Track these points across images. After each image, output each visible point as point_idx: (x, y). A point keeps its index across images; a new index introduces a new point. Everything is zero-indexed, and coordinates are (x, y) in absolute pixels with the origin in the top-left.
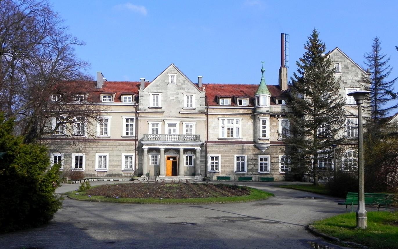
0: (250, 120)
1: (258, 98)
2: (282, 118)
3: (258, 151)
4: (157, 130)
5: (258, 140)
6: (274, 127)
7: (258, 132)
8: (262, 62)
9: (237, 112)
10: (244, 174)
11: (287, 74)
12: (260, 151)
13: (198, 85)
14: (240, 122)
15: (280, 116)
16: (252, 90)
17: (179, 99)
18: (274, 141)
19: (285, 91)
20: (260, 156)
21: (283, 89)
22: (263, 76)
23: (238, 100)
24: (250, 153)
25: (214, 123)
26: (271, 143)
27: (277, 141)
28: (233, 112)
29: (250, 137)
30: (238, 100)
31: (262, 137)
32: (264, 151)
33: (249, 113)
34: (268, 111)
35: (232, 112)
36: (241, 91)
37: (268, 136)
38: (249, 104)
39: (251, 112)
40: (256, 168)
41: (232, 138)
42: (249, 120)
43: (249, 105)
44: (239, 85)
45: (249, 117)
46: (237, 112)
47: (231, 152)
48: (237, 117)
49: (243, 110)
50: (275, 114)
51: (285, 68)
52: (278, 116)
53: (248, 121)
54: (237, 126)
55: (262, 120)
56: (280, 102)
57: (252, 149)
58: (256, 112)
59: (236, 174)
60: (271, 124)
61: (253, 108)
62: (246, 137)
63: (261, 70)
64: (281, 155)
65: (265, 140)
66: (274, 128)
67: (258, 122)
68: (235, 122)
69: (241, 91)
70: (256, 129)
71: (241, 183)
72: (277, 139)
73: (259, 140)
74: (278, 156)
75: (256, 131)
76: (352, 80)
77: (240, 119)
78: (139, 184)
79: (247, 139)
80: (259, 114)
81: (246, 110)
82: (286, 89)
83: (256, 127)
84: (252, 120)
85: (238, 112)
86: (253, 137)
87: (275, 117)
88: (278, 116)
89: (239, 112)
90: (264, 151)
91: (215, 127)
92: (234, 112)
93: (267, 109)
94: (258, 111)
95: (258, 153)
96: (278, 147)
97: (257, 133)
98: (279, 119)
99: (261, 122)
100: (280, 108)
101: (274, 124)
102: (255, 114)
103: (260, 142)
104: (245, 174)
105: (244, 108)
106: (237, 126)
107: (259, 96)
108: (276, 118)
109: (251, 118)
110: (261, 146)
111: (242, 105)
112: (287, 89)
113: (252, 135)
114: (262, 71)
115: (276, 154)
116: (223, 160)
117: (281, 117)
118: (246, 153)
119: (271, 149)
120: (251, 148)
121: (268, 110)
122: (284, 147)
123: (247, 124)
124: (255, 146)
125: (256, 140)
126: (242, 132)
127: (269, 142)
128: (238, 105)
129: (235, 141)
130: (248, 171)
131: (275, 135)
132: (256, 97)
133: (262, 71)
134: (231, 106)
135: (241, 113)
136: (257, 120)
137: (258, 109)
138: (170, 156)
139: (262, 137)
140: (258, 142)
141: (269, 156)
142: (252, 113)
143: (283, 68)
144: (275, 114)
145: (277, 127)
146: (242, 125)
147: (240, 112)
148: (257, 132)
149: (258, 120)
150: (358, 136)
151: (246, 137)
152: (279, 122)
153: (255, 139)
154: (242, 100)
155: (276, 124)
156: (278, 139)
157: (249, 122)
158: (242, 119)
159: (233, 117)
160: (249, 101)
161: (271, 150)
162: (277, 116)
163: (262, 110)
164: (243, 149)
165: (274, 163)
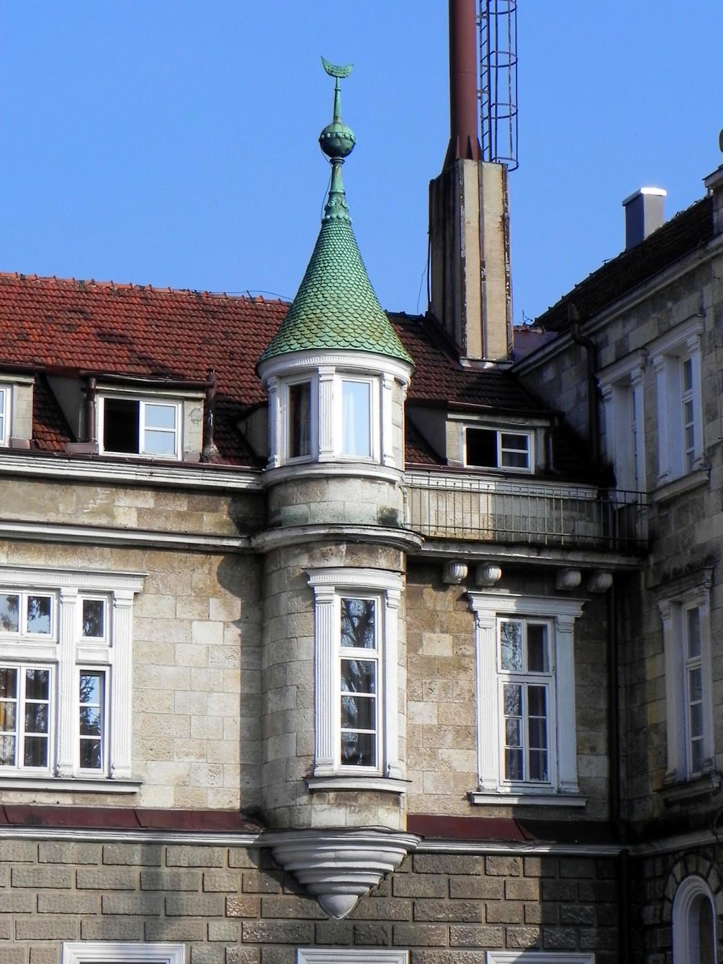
0: (213, 602)
1: (302, 397)
2: (505, 592)
3: (288, 903)
5: (297, 795)
6: (431, 674)
7: (300, 721)
8: (332, 62)
9: (93, 513)
11: (505, 221)
12: (314, 909)
14: (120, 620)
15: (495, 573)
16: (207, 341)
18: (437, 810)
19: (488, 365)
21: (473, 349)
22: (339, 188)
23: (100, 403)
26: (420, 824)
27: (461, 810)
28: (52, 518)
29: (216, 770)
30: (100, 403)
31: (338, 767)
32: (347, 902)
33: (207, 529)
34: (388, 520)
35: (41, 509)
36: (105, 337)
37: (392, 758)
38: (206, 443)
39: (222, 524)
41: (90, 773)
42: (201, 596)
43: (203, 457)
44: (84, 290)
45: (205, 572)
46: (93, 513)
47: (36, 918)
48: (97, 566)
49: (147, 500)
50: (453, 550)
51: (492, 172)
52: (476, 568)
53: (198, 607)
54: (95, 650)
55: (337, 599)
56: (481, 449)
57: (236, 886)
58: (278, 525)
60: (413, 643)
61: (240, 482)
62: (176, 768)
63: (321, 141)
64: (508, 947)
65: (363, 799)
66: (439, 683)
67: (298, 623)
68: (72, 615)
69: (105, 337)
70: (282, 689)
72: (462, 790)
73: (304, 799)
74: (481, 953)
75: (271, 706)
77: (124, 589)
78: (706, 244)
79: (182, 784)
80: (306, 546)
81: (181, 504)
82: (498, 348)
83: (283, 665)
84: (238, 603)
85: (103, 521)
86: (244, 768)
87: (442, 586)
88: (476, 568)
89: (112, 516)
90: (347, 902)
92: (61, 519)
93: (389, 498)
94: (296, 510)
95: (293, 929)
96: (479, 868)
97: (286, 724)
98: (477, 603)
99: (331, 616)
100: (486, 505)
101: (439, 646)
102: (270, 539)
103: (326, 815)
105: (161, 477)
106: (95, 650)
107: (314, 370)
108: (449, 596)
109: (227, 581)
110: (329, 857)
111: (137, 452)
112: (511, 355)
113: (230, 748)
114: (333, 148)
117: (498, 584)
118: (185, 922)
119: (421, 886)
120: (225, 880)
121: (393, 512)
122: (535, 867)
123: (189, 639)
124: (267, 859)
125: (278, 799)
127: (394, 819)
128: (101, 451)
129: (66, 801)
131: (443, 753)
132: (282, 376)
133: (333, 148)
134: (36, 450)
135: (133, 524)
136: (291, 602)
137: (293, 491)
138: (87, 944)
139: (338, 767)
140: (302, 819)
142: (233, 529)
143: (469, 169)
144: (453, 550)
145: (463, 679)
146: (137, 644)
147: (121, 521)
148: (284, 714)
149: (298, 603)
151: (176, 768)
152: (480, 632)
153: (259, 793)
154: (143, 405)
155: (454, 645)
156: (469, 797)
157: (205, 617)
158: (137, 585)
159: (55, 563)
160: (206, 415)
161: (414, 899)
162: (462, 571)
163: (338, 507)
164: (150, 885)
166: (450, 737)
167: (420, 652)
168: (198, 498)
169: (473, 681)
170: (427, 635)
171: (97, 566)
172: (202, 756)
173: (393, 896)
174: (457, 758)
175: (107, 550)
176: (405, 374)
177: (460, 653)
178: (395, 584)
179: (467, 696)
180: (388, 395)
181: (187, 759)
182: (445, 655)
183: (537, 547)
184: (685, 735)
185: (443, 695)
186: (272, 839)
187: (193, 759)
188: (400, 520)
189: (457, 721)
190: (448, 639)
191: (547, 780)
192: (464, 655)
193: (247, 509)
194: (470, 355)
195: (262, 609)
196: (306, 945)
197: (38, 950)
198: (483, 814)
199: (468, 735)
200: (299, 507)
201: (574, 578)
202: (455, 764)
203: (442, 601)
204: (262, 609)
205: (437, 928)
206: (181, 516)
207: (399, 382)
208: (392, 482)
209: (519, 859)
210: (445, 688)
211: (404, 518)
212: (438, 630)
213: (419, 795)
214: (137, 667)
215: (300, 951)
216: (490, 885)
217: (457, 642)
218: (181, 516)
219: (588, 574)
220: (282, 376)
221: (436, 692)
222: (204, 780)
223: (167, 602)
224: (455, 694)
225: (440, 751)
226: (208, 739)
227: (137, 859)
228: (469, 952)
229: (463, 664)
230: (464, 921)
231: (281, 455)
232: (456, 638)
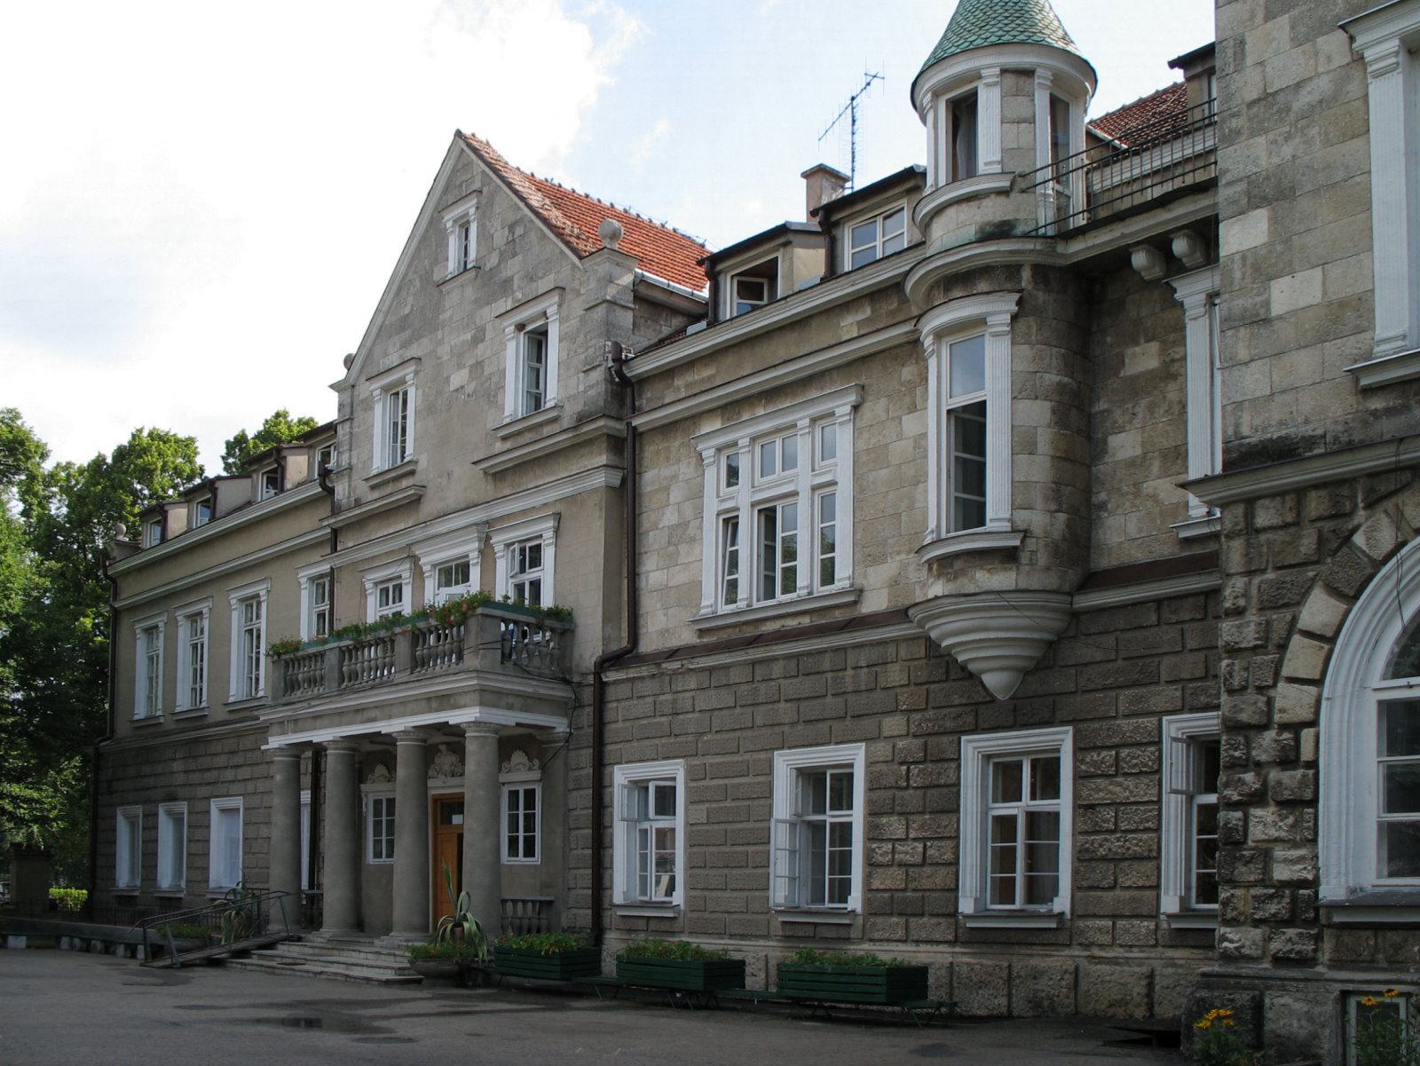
4: (536, 585)
10: (842, 932)
13: (1207, 53)
17: (289, 419)
20: (972, 748)
24: (893, 725)
25: (672, 499)
40: (941, 877)
41: (732, 607)
59: (787, 938)
65: (958, 564)
71: (463, 996)
74: (1154, 720)
76: (462, 286)
91: (679, 525)
96: (1153, 618)
104: (848, 940)
115: (1140, 699)
116: (701, 813)
123: (900, 437)
126: (783, 547)
130: (875, 908)
141: (1063, 740)
150: (1287, 498)
165: (1109, 814)
166: (1156, 466)
167: (1122, 374)
169: (1183, 390)
173: (908, 685)
175: (835, 373)
177: (1167, 360)
179: (1176, 409)
181: (898, 558)
182: (1151, 367)
184: (294, 703)
185: (1148, 417)
187: (903, 556)
190: (1154, 347)
192: (1173, 361)
193: (605, 457)
196: (778, 749)
197: (711, 765)
202: (1162, 496)
205: (1105, 697)
206: (893, 313)
212: (1142, 340)
213: (1121, 542)
214: (857, 477)
215: (964, 738)
216: (1168, 635)
217: (1165, 347)
221: (1140, 416)
224: (1162, 412)
225: (1145, 485)
226: (917, 533)
228: (1140, 720)
230: (1135, 684)
232: (1164, 342)
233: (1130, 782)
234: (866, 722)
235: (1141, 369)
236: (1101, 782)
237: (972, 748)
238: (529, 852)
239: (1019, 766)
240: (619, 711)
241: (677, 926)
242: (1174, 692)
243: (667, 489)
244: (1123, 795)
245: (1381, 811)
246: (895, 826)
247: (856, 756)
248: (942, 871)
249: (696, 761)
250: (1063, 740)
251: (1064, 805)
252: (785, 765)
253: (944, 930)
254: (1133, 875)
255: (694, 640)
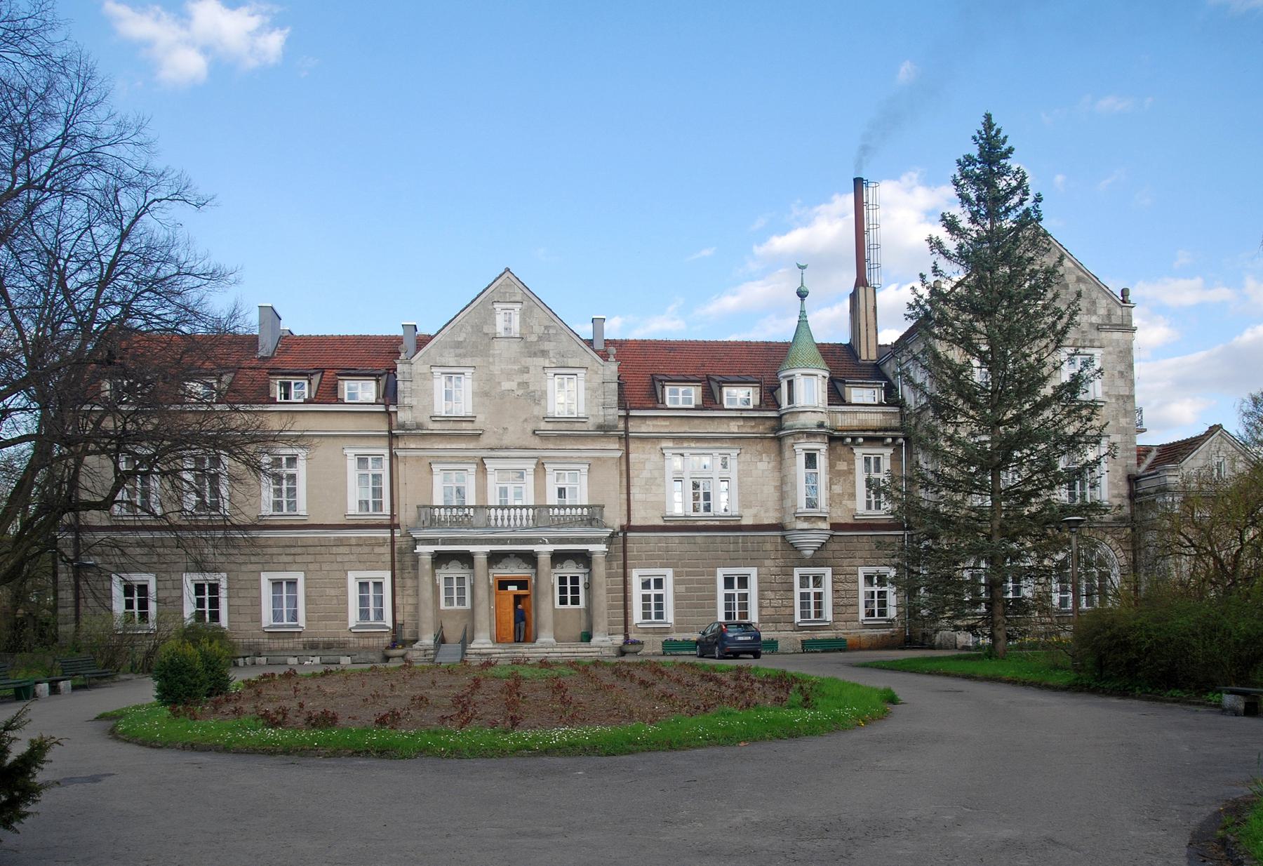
6: (839, 476)
15: (861, 440)
20: (797, 572)
21: (864, 357)
24: (767, 562)
26: (835, 527)
27: (850, 521)
34: (821, 425)
40: (788, 611)
41: (707, 514)
49: (741, 423)
50: (845, 433)
52: (854, 439)
53: (760, 457)
58: (784, 429)
60: (831, 466)
62: (754, 511)
65: (813, 519)
75: (784, 489)
77: (734, 453)
79: (755, 516)
88: (854, 439)
90: (809, 553)
96: (856, 540)
99: (801, 460)
101: (842, 466)
121: (823, 423)
123: (756, 468)
127: (824, 525)
129: (717, 523)
131: (844, 502)
132: (784, 377)
141: (828, 572)
143: (862, 290)
144: (845, 433)
151: (754, 511)
157: (761, 460)
166: (846, 497)
168: (757, 420)
169: (854, 477)
170: (838, 463)
171: (724, 445)
172: (762, 506)
174: (849, 504)
176: (827, 374)
178: (824, 447)
180: (820, 382)
183: (875, 431)
186: (785, 533)
188: (825, 424)
189: (849, 491)
190: (845, 463)
191: (381, 511)
194: (862, 358)
195: (781, 457)
198: (858, 522)
199: (852, 496)
200: (788, 422)
201: (889, 440)
203: (841, 450)
204: (781, 457)
206: (752, 427)
207: (824, 377)
208: (822, 412)
209: (511, 501)
210: (845, 480)
211: (827, 423)
218: (752, 427)
219: (894, 439)
220: (784, 377)
222: (762, 514)
223: (748, 456)
227: (740, 541)
229: (851, 472)
231: (785, 404)
233: (849, 584)
234: (757, 561)
235: (842, 469)
236: (841, 584)
237: (797, 572)
238: (575, 601)
239: (808, 578)
240: (633, 549)
241: (302, 635)
242: (862, 560)
243: (644, 463)
244: (847, 588)
245: (664, 580)
246: (770, 594)
247: (753, 573)
248: (789, 609)
249: (678, 570)
250: (828, 572)
251: (798, 590)
252: (721, 573)
253: (789, 627)
254: (851, 610)
255: (662, 523)
